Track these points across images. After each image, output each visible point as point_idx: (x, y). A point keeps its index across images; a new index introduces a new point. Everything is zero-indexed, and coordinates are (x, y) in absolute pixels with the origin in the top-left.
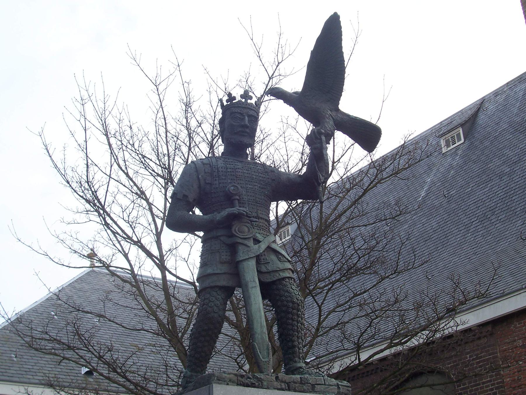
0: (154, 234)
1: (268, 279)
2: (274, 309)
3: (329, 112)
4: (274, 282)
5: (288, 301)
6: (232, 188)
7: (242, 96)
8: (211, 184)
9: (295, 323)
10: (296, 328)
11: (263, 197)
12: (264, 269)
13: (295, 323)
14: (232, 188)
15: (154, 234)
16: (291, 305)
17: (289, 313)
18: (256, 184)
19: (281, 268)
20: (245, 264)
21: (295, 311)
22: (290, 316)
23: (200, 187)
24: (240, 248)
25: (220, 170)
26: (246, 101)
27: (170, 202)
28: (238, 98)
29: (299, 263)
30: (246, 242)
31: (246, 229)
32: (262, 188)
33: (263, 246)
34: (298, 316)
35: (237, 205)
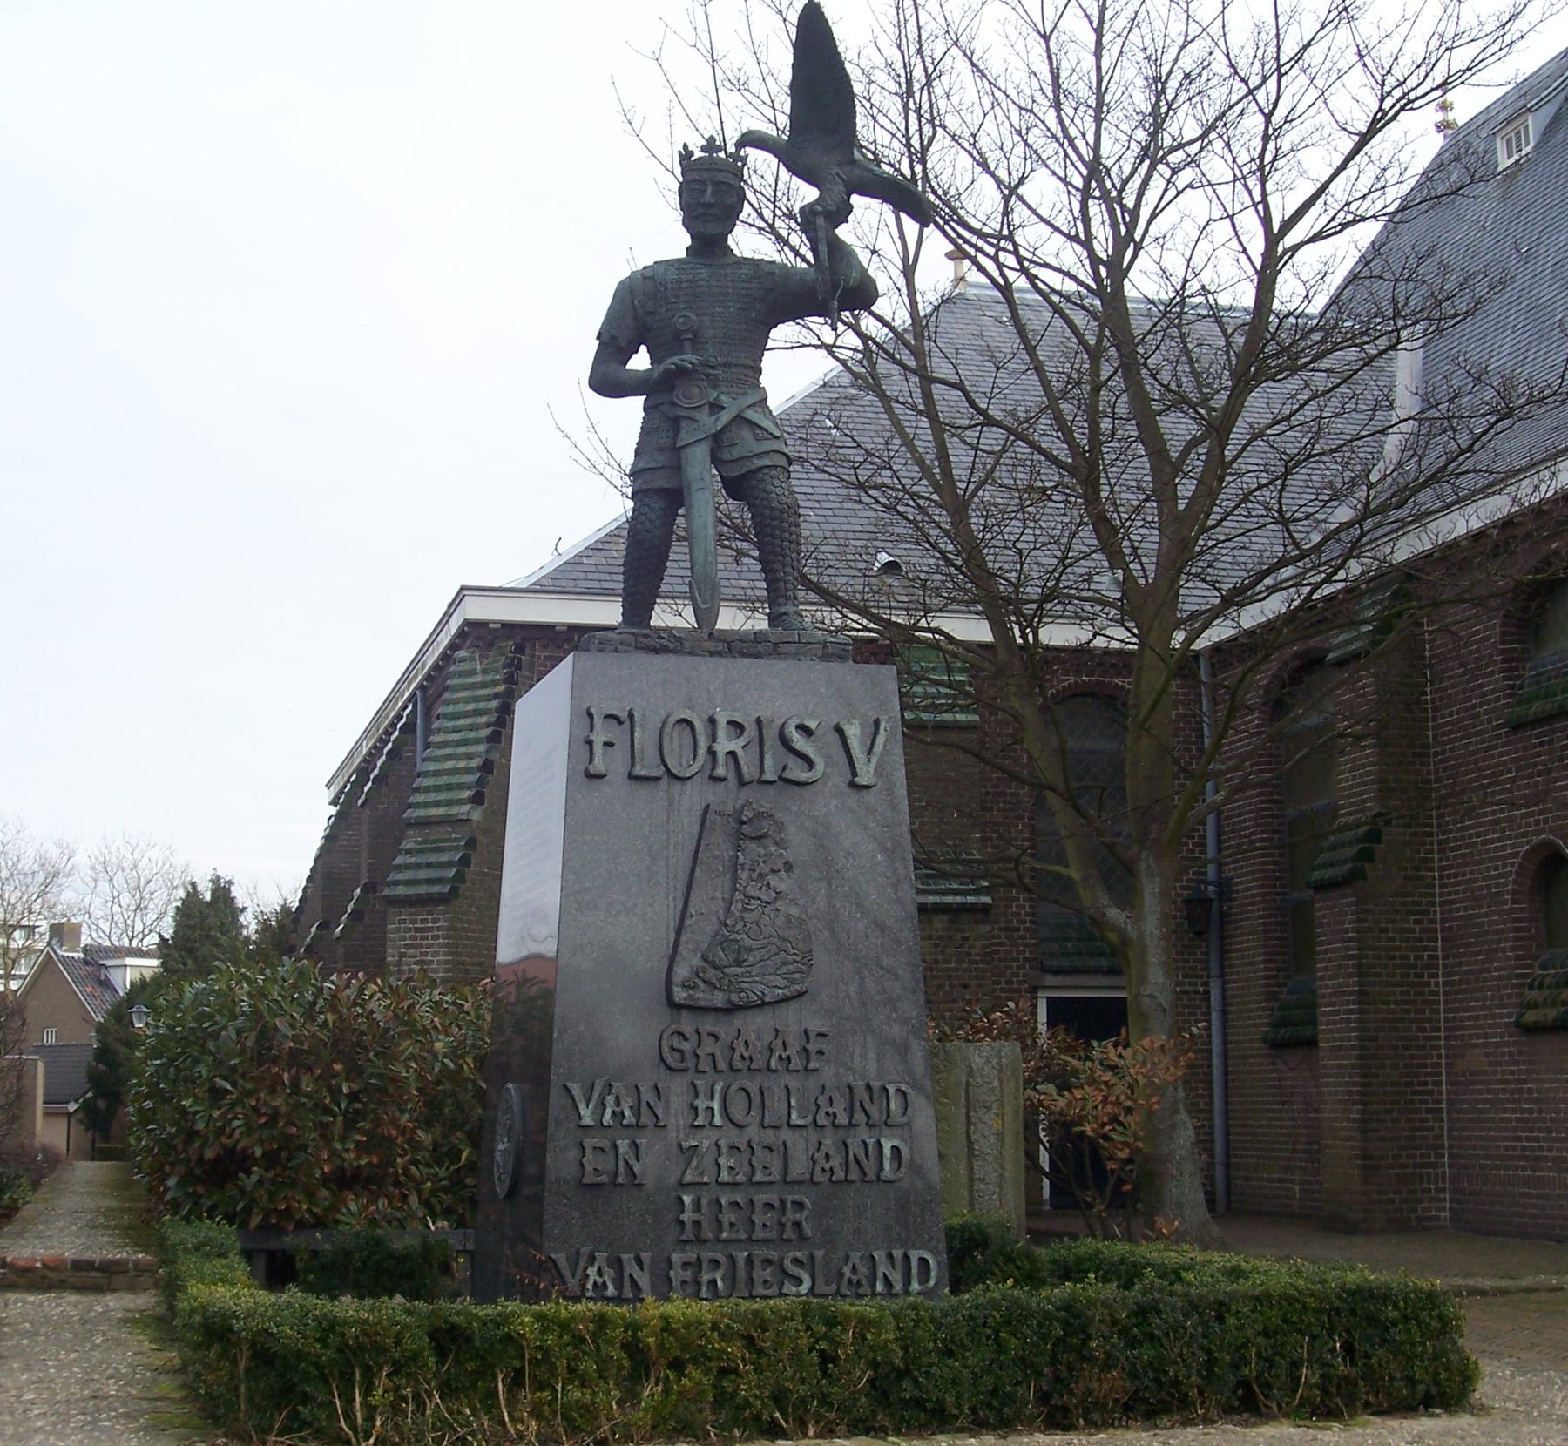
0: (1088, 144)
1: (733, 472)
2: (1179, 636)
3: (836, 169)
4: (744, 476)
5: (765, 507)
6: (681, 320)
7: (703, 149)
8: (652, 313)
9: (778, 542)
10: (779, 550)
11: (744, 326)
12: (726, 456)
13: (778, 542)
14: (681, 320)
15: (1088, 144)
16: (767, 512)
17: (767, 526)
18: (731, 304)
19: (757, 452)
20: (689, 450)
21: (776, 523)
22: (768, 530)
23: (636, 319)
24: (683, 424)
25: (669, 286)
26: (711, 155)
27: (746, 203)
28: (698, 154)
29: (1110, 420)
30: (696, 415)
31: (696, 391)
32: (745, 310)
33: (725, 417)
34: (783, 530)
35: (689, 350)
